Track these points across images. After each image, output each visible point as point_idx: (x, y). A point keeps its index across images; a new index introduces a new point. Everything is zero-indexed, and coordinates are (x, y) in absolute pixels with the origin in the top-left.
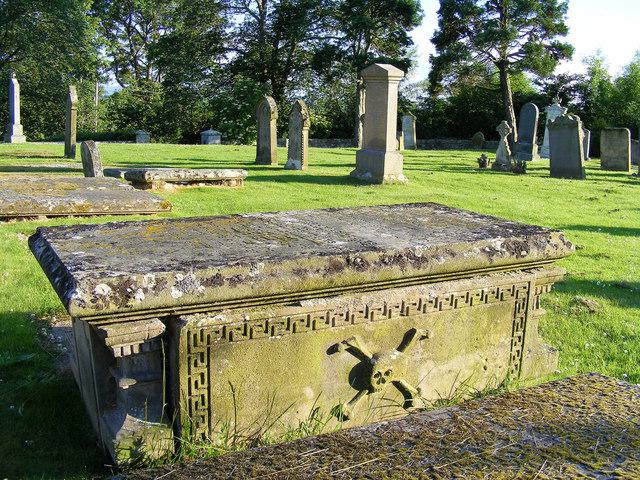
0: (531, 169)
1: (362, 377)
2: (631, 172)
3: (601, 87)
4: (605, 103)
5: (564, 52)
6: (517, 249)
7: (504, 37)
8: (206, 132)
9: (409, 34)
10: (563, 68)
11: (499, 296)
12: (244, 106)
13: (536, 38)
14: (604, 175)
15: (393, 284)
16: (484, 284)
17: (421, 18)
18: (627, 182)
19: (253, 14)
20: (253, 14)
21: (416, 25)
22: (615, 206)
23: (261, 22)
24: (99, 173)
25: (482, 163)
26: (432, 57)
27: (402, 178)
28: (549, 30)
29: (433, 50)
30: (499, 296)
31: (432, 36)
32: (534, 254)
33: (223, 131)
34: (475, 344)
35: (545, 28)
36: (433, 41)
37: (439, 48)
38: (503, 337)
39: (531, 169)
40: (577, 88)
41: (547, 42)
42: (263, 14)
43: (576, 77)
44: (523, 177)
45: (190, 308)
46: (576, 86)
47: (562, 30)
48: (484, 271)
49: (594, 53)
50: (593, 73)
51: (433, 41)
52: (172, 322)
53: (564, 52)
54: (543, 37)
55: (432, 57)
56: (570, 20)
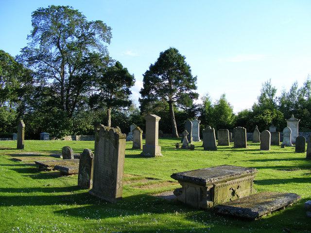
0: (197, 147)
1: (233, 193)
2: (230, 146)
3: (209, 110)
4: (211, 116)
5: (195, 96)
6: (251, 172)
7: (172, 91)
8: (43, 133)
9: (130, 89)
10: (196, 102)
11: (249, 180)
12: (59, 122)
13: (183, 90)
14: (223, 148)
15: (236, 178)
16: (247, 178)
17: (134, 82)
18: (232, 151)
19: (58, 79)
20: (58, 79)
21: (132, 85)
22: (235, 161)
23: (62, 83)
24: (73, 157)
25: (177, 146)
26: (140, 99)
27: (161, 154)
28: (188, 88)
29: (140, 96)
30: (249, 180)
31: (140, 90)
32: (253, 172)
33: (50, 132)
34: (246, 188)
35: (186, 86)
36: (140, 92)
37: (143, 95)
38: (249, 187)
39: (197, 147)
40: (199, 109)
41: (187, 92)
42: (63, 79)
43: (198, 105)
44: (194, 151)
45: (217, 183)
46: (199, 109)
47: (194, 88)
48: (246, 176)
49: (206, 95)
50: (205, 103)
51: (140, 92)
52: (214, 186)
53: (195, 96)
54: (186, 90)
55: (140, 99)
56: (198, 84)
